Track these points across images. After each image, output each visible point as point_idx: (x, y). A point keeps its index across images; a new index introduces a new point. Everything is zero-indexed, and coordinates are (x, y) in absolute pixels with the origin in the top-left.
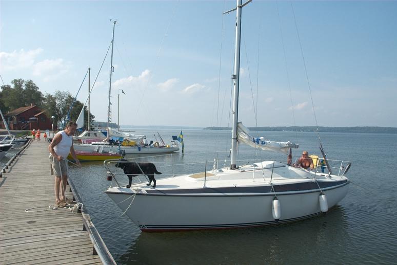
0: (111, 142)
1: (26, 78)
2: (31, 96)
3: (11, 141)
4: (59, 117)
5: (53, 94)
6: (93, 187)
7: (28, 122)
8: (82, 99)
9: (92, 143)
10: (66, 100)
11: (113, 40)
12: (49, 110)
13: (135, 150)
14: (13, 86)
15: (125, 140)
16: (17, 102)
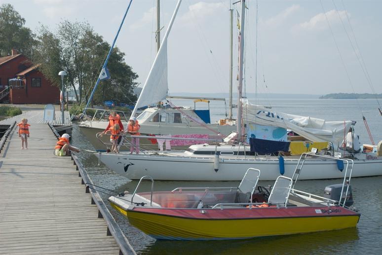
2: (10, 36)
5: (54, 30)
6: (8, 111)
7: (7, 87)
9: (195, 148)
12: (48, 63)
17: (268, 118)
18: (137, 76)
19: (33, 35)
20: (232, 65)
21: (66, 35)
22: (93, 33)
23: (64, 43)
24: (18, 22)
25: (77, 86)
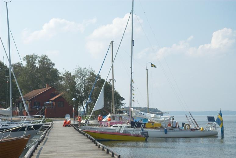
0: (133, 124)
1: (40, 54)
3: (42, 121)
4: (80, 101)
7: (43, 107)
8: (105, 76)
10: (88, 79)
11: (133, 10)
12: (68, 92)
13: (161, 133)
14: (24, 64)
15: (151, 122)
16: (29, 83)
17: (140, 115)
18: (124, 99)
19: (59, 73)
20: (148, 94)
21: (79, 75)
22: (95, 74)
23: (78, 80)
24: (51, 66)
25: (85, 106)
